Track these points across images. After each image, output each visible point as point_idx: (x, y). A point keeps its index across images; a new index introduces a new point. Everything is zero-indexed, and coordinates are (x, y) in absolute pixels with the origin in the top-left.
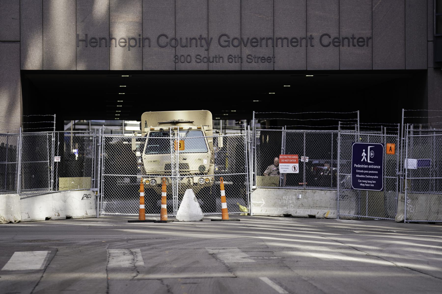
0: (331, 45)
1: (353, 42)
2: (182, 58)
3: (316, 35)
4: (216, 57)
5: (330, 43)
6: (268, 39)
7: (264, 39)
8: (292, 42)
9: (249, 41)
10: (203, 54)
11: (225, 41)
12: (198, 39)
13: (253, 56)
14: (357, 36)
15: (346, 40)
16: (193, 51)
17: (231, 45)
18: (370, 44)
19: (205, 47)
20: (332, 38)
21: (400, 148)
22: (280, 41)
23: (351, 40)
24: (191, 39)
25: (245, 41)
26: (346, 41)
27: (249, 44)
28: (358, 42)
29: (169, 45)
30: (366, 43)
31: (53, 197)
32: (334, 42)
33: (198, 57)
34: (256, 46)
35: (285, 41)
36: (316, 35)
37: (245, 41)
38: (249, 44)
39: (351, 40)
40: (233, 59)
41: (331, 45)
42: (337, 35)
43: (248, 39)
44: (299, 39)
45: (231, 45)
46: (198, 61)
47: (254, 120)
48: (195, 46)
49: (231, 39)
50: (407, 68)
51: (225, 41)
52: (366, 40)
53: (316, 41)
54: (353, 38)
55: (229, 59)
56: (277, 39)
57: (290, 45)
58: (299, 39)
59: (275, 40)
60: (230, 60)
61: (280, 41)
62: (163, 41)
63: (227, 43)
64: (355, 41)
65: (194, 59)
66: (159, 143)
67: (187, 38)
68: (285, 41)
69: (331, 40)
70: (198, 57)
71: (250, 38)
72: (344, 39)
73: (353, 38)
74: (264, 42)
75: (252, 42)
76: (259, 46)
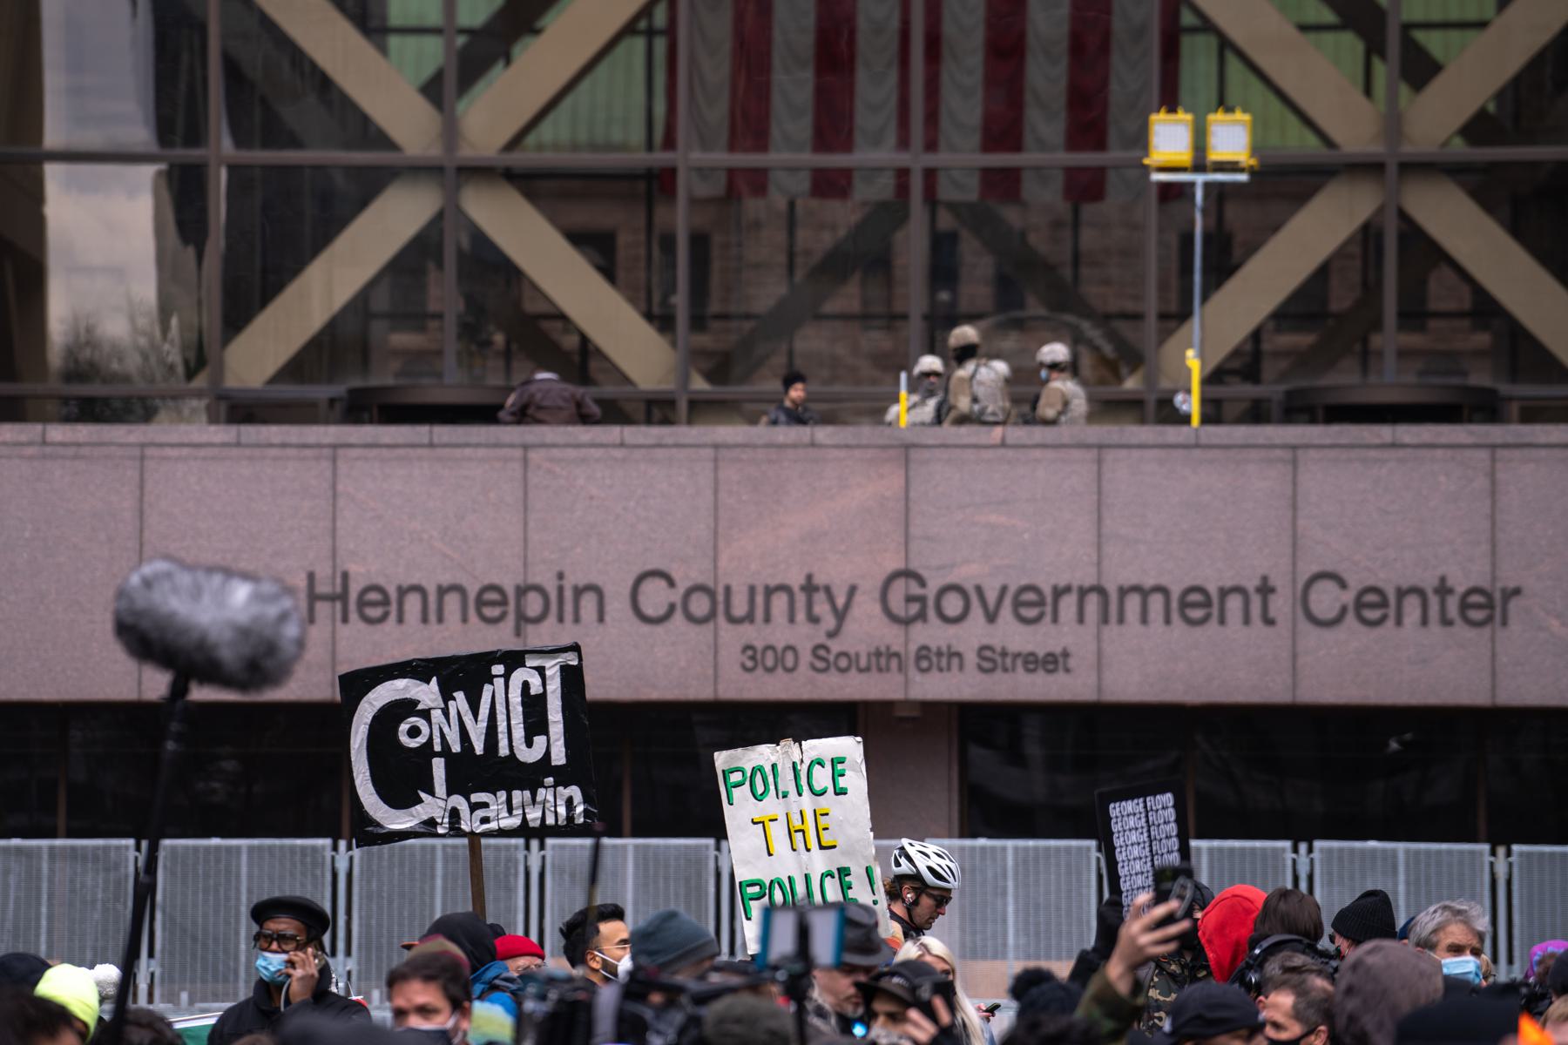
0: (1350, 617)
1: (810, 605)
2: (770, 654)
4: (878, 654)
5: (672, 608)
6: (1083, 592)
7: (1068, 589)
8: (1184, 605)
9: (1008, 601)
12: (796, 589)
13: (934, 649)
14: (1460, 585)
15: (1412, 603)
17: (931, 613)
20: (682, 587)
21: (292, 875)
22: (1133, 602)
23: (1434, 602)
24: (769, 592)
25: (991, 597)
26: (1412, 605)
27: (1006, 611)
28: (1464, 606)
29: (678, 616)
32: (1360, 605)
33: (822, 653)
34: (1204, 621)
35: (1156, 602)
37: (991, 597)
38: (1006, 611)
39: (1434, 602)
40: (934, 659)
41: (1350, 617)
43: (1004, 590)
44: (393, 595)
45: (931, 613)
46: (820, 665)
48: (1161, 618)
49: (931, 592)
51: (910, 599)
52: (1049, 600)
54: (1443, 590)
57: (1175, 616)
58: (393, 595)
59: (432, 599)
60: (925, 664)
62: (655, 597)
63: (914, 608)
64: (1453, 604)
68: (1156, 602)
70: (822, 653)
71: (1012, 589)
73: (810, 587)
74: (1068, 604)
75: (1017, 604)
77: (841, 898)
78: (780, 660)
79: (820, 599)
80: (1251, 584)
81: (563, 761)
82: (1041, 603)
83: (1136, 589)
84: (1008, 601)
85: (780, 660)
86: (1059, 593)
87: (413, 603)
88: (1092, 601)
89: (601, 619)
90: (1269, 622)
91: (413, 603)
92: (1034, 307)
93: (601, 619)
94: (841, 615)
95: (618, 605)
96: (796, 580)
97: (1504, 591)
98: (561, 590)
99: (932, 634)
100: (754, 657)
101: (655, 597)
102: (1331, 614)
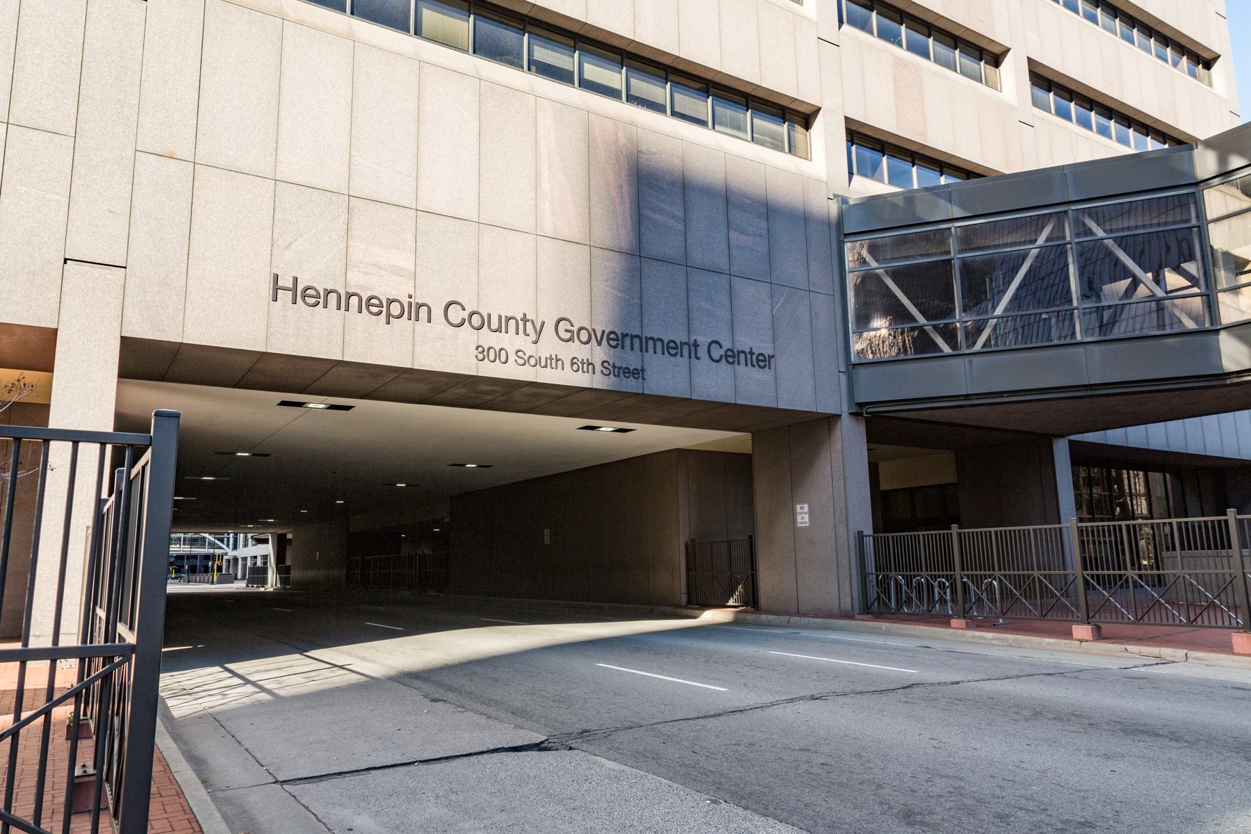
2: (492, 358)
3: (703, 340)
6: (633, 337)
10: (530, 349)
11: (567, 331)
14: (756, 352)
15: (742, 356)
16: (510, 341)
18: (773, 366)
19: (533, 337)
23: (521, 323)
24: (508, 319)
27: (604, 342)
28: (758, 360)
30: (321, 300)
31: (37, 636)
32: (727, 356)
35: (659, 344)
36: (703, 340)
38: (604, 342)
39: (521, 323)
42: (730, 346)
43: (603, 332)
46: (521, 361)
47: (1070, 520)
49: (575, 329)
51: (567, 331)
53: (702, 351)
54: (752, 353)
55: (573, 364)
56: (647, 339)
61: (651, 342)
64: (754, 357)
65: (512, 357)
66: (1235, 608)
67: (500, 317)
68: (659, 344)
69: (465, 315)
72: (739, 352)
75: (609, 339)
76: (321, 304)
77: (54, 424)
79: (529, 324)
80: (747, 350)
81: (748, 436)
82: (617, 339)
83: (652, 338)
87: (333, 298)
88: (637, 341)
89: (429, 321)
90: (698, 358)
91: (333, 298)
92: (901, 203)
93: (429, 321)
94: (539, 334)
95: (438, 313)
96: (747, 350)
97: (325, 290)
98: (410, 304)
100: (483, 353)
101: (456, 314)
102: (458, 321)
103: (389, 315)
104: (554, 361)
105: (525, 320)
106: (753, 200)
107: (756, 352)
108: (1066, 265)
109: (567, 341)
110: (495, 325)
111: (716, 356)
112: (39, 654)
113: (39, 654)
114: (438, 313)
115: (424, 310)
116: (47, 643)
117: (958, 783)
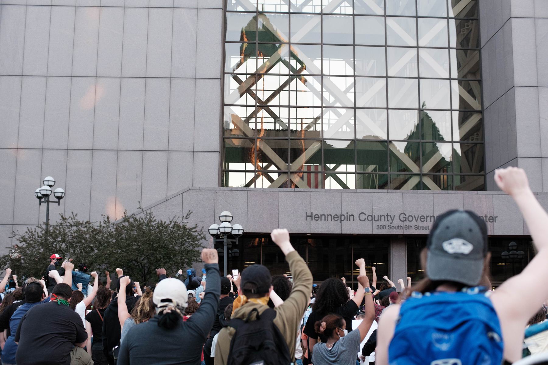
19: (391, 221)
20: (367, 215)
49: (407, 217)
50: (343, 233)
75: (421, 219)
78: (383, 227)
82: (424, 218)
84: (419, 219)
85: (383, 227)
86: (427, 217)
94: (392, 220)
99: (407, 223)
101: (363, 217)
102: (363, 219)
103: (341, 220)
104: (399, 227)
105: (387, 216)
106: (256, 362)
107: (488, 216)
108: (200, 358)
109: (403, 221)
110: (376, 219)
111: (362, 218)
112: (289, 121)
113: (289, 121)
114: (356, 217)
115: (352, 217)
116: (291, 122)
117: (455, 306)
